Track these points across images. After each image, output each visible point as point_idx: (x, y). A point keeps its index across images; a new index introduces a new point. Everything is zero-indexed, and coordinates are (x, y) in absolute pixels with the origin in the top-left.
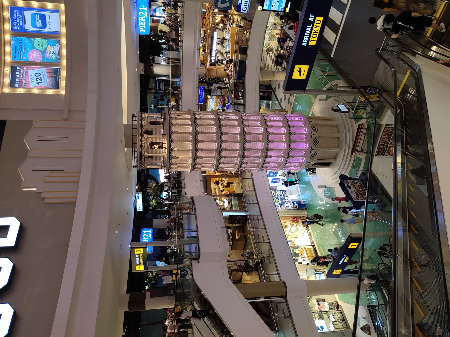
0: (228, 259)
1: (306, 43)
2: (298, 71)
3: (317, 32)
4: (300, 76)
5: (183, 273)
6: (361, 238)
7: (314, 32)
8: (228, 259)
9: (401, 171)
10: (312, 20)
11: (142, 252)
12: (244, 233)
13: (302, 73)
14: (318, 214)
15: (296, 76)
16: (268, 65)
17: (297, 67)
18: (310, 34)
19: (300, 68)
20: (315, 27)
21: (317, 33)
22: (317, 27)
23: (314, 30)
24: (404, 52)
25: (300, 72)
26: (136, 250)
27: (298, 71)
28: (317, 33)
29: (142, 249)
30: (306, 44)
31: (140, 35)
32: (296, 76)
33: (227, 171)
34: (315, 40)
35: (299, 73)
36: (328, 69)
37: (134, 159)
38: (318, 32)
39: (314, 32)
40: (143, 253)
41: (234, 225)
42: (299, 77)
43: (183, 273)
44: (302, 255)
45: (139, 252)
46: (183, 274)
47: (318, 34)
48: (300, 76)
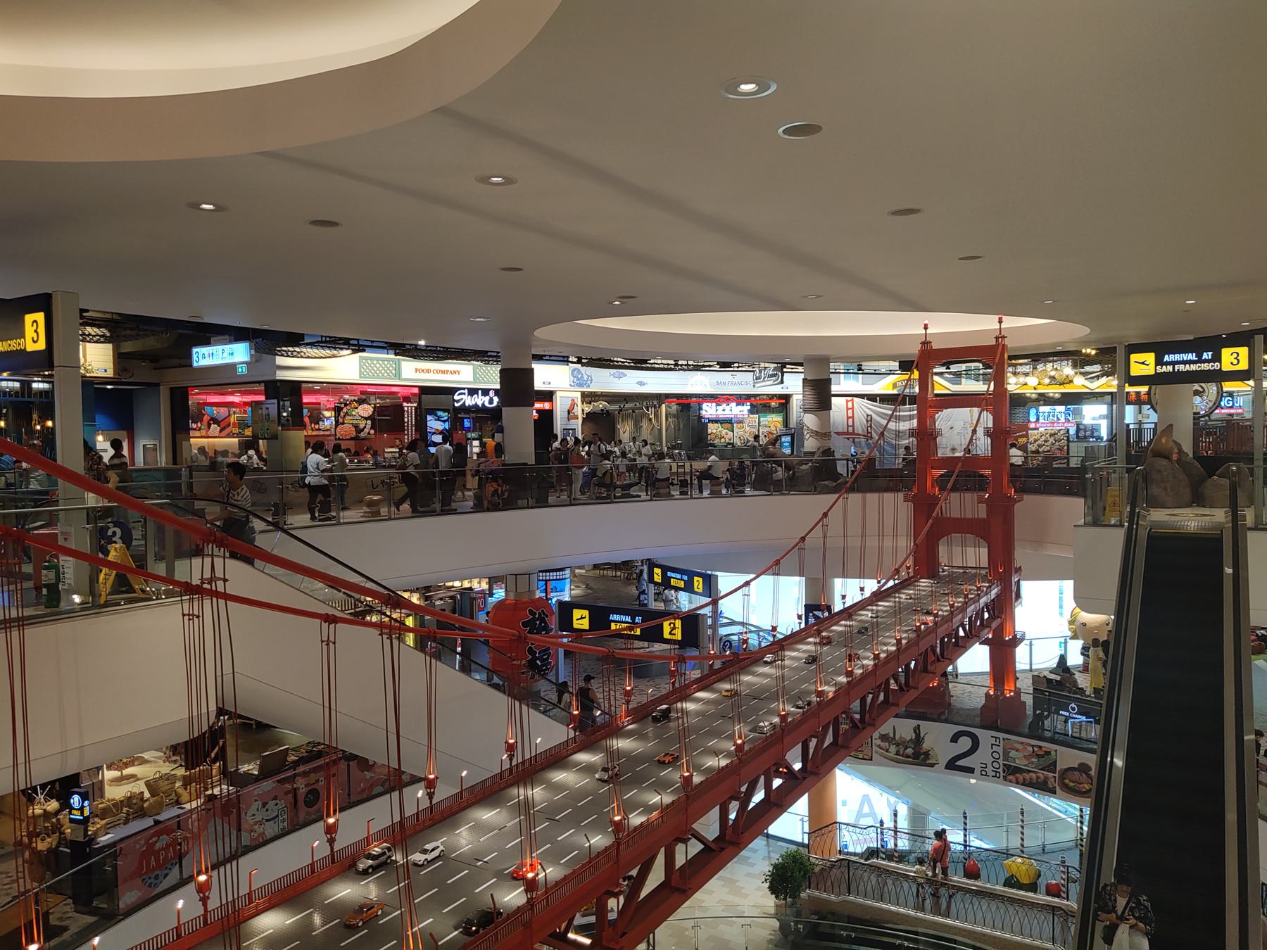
0: (981, 763)
4: (578, 619)
5: (114, 533)
6: (1219, 539)
8: (981, 763)
9: (872, 498)
11: (31, 347)
13: (580, 621)
15: (577, 613)
17: (586, 613)
19: (585, 618)
24: (567, 925)
25: (582, 618)
26: (40, 317)
29: (41, 345)
32: (577, 613)
35: (580, 617)
36: (1046, 743)
37: (332, 639)
40: (29, 349)
43: (114, 533)
44: (1107, 625)
45: (29, 331)
46: (110, 533)
48: (578, 619)
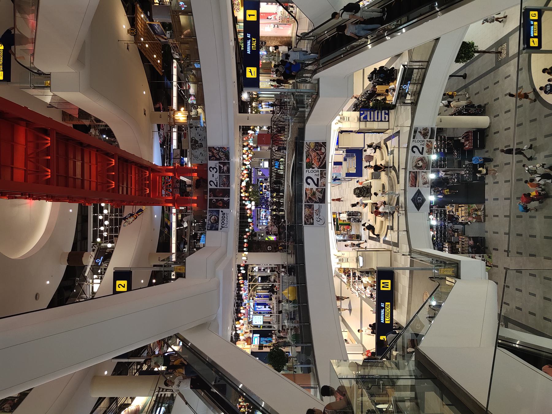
10: (383, 306)
18: (384, 315)
19: (250, 70)
25: (251, 72)
35: (250, 73)
42: (252, 68)
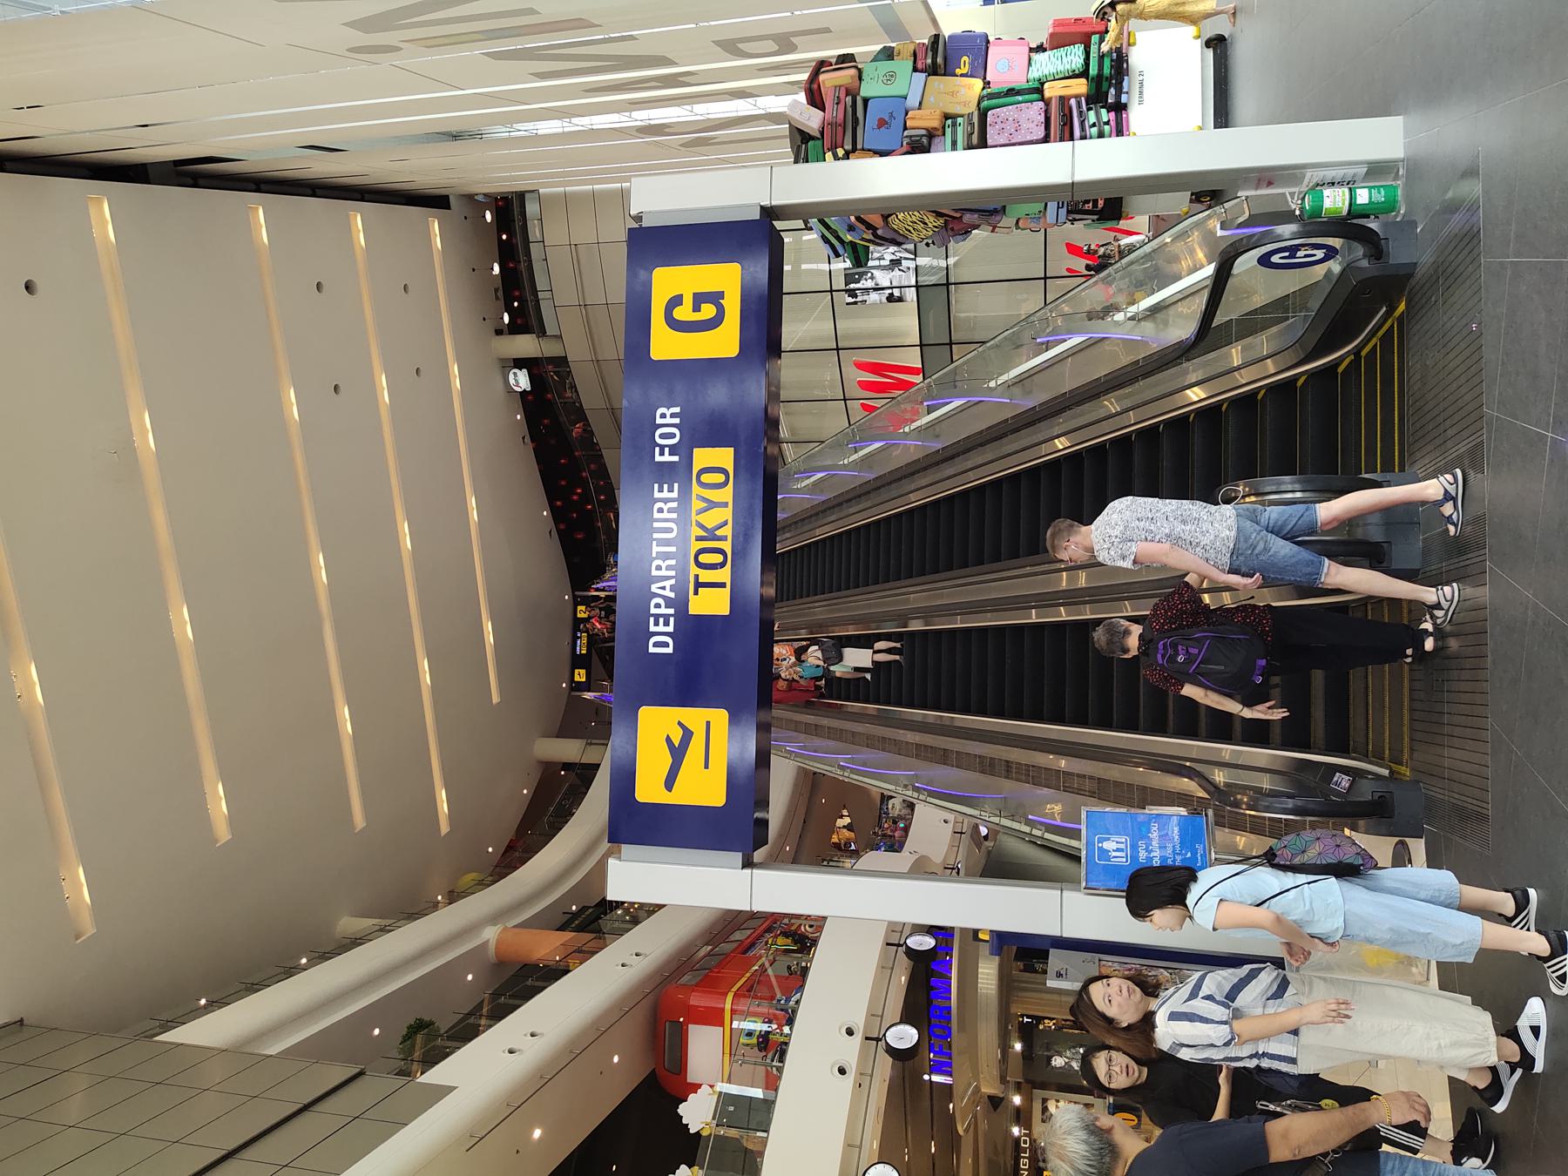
1: (673, 582)
2: (668, 740)
3: (718, 533)
7: (699, 539)
12: (1486, 608)
14: (686, 1101)
16: (1565, 959)
20: (697, 505)
21: (724, 538)
22: (712, 505)
23: (702, 527)
27: (668, 740)
28: (724, 538)
30: (672, 588)
31: (1122, 198)
33: (1119, 108)
34: (723, 585)
35: (668, 760)
38: (727, 531)
39: (699, 539)
41: (574, 925)
47: (727, 546)
